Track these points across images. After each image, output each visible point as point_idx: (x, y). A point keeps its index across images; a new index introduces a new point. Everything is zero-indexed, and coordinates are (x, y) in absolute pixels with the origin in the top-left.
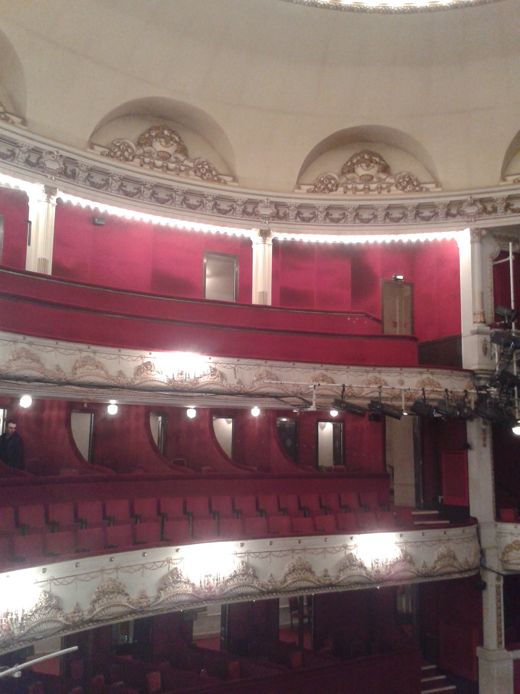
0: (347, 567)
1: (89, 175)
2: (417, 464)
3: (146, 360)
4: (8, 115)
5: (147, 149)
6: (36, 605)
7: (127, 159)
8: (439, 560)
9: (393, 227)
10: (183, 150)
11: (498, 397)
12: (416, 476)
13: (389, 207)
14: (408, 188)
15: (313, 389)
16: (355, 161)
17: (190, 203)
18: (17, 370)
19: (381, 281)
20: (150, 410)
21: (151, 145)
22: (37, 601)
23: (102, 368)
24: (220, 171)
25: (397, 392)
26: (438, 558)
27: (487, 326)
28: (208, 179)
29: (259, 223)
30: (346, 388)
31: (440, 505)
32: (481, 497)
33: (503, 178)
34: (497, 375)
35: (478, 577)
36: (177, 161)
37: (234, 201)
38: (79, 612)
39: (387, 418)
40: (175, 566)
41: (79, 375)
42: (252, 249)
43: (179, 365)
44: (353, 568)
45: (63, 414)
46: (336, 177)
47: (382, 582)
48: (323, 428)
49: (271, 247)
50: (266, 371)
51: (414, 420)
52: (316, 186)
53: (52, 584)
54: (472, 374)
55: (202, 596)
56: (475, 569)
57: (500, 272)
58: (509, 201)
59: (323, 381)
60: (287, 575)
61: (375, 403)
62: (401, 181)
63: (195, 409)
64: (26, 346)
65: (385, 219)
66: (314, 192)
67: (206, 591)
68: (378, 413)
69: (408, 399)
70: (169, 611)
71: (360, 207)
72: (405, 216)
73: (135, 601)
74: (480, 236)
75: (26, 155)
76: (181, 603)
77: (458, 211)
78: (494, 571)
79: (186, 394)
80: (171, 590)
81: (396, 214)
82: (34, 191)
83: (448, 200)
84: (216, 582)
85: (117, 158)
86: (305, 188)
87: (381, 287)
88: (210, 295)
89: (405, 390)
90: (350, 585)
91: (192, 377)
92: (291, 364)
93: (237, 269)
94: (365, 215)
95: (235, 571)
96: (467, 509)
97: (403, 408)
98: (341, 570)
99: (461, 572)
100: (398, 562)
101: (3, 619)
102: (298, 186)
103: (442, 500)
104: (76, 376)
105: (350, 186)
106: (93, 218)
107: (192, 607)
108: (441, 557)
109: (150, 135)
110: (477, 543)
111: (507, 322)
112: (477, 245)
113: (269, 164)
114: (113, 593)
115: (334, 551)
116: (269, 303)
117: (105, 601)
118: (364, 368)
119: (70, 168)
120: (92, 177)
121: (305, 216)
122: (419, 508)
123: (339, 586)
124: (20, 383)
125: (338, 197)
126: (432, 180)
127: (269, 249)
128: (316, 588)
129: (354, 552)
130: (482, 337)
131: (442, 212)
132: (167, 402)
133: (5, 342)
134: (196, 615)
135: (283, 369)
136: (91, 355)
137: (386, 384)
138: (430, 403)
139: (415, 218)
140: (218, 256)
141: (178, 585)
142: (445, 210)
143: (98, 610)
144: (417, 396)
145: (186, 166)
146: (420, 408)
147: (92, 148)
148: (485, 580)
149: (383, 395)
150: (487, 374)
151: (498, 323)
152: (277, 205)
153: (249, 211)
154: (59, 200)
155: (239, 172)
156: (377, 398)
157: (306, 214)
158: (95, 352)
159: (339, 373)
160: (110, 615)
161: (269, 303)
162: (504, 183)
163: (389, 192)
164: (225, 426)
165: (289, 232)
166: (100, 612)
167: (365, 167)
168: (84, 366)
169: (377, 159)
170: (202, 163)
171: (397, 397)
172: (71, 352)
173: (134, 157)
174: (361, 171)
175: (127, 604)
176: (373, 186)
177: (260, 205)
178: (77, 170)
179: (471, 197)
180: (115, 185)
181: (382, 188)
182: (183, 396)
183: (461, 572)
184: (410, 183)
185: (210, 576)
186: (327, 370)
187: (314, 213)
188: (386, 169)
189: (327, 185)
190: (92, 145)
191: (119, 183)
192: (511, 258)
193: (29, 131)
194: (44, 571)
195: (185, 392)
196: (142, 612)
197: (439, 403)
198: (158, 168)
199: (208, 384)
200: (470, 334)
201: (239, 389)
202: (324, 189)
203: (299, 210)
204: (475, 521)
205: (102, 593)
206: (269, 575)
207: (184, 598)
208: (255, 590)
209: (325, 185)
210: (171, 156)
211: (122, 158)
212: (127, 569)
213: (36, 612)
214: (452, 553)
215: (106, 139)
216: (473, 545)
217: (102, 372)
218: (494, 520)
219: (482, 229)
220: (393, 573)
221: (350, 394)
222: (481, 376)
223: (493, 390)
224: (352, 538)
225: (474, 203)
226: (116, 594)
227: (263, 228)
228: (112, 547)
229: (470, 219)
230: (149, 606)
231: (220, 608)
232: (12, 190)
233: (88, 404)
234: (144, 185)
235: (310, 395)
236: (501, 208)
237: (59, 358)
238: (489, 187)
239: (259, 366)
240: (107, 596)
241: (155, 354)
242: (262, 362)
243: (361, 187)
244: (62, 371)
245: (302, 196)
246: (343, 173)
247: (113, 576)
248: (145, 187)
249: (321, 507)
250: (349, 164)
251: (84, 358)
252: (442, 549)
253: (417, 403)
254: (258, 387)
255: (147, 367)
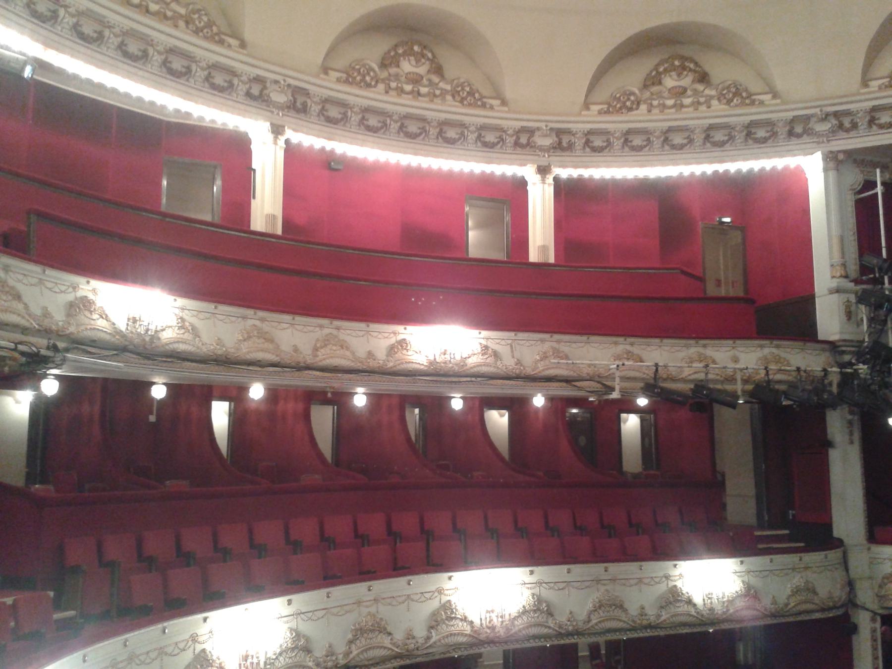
0: (671, 603)
1: (323, 107)
2: (764, 468)
3: (80, 293)
4: (223, 37)
5: (393, 70)
6: (281, 646)
7: (368, 86)
8: (793, 595)
9: (716, 154)
10: (438, 70)
11: (869, 377)
12: (757, 485)
13: (711, 127)
14: (735, 101)
15: (615, 370)
16: (661, 69)
17: (445, 135)
18: (248, 353)
19: (701, 225)
20: (406, 400)
21: (398, 66)
22: (282, 641)
23: (348, 348)
24: (485, 93)
25: (729, 372)
26: (792, 591)
27: (851, 281)
28: (470, 105)
29: (537, 157)
30: (659, 369)
31: (789, 520)
32: (848, 512)
33: (865, 83)
34: (867, 347)
35: (846, 617)
36: (431, 83)
37: (502, 130)
38: (332, 655)
39: (716, 407)
40: (448, 598)
41: (320, 357)
42: (527, 191)
43: (444, 343)
44: (678, 605)
45: (300, 406)
46: (637, 92)
47: (718, 623)
48: (626, 420)
49: (552, 187)
50: (552, 348)
51: (752, 409)
52: (609, 105)
53: (299, 619)
54: (833, 346)
55: (483, 637)
56: (842, 606)
57: (864, 209)
58: (873, 114)
59: (628, 359)
60: (590, 613)
61: (700, 387)
62: (725, 92)
63: (461, 398)
64: (258, 323)
65: (704, 144)
66: (607, 112)
67: (488, 631)
68: (703, 401)
69: (745, 381)
70: (442, 656)
71: (670, 130)
72: (731, 138)
73: (400, 643)
74: (834, 161)
75: (247, 86)
76: (458, 646)
77: (804, 128)
78: (867, 610)
79: (450, 379)
80: (444, 629)
81: (719, 136)
82: (255, 128)
83: (791, 114)
84: (500, 620)
85: (357, 84)
86: (595, 108)
87: (700, 231)
88: (474, 251)
89: (741, 370)
90: (675, 627)
91: (458, 358)
92: (584, 338)
93: (508, 218)
94: (678, 139)
95: (524, 607)
96: (829, 526)
97: (739, 393)
98: (662, 607)
99: (823, 610)
100: (739, 596)
101: (242, 663)
102: (586, 106)
103: (793, 516)
104: (318, 359)
105: (655, 103)
106: (329, 163)
107: (471, 652)
108: (796, 591)
109: (396, 53)
110: (844, 573)
111: (877, 275)
112: (832, 174)
113: (546, 78)
114: (372, 631)
115: (652, 583)
116: (552, 260)
117: (362, 642)
118: (683, 342)
119: (300, 100)
120: (327, 111)
121: (596, 145)
122: (761, 527)
123: (661, 628)
124: (251, 368)
125: (640, 118)
126: (767, 89)
127: (550, 190)
128: (629, 630)
129: (679, 584)
130: (844, 297)
131: (782, 131)
132: (429, 390)
133: (233, 319)
134: (476, 662)
135: (574, 345)
136: (335, 332)
137: (714, 362)
138: (777, 387)
139: (746, 140)
140: (482, 203)
141: (452, 623)
142: (787, 128)
143: (355, 653)
144: (758, 377)
145: (442, 89)
146: (763, 394)
147: (326, 73)
148: (855, 621)
149: (710, 376)
150: (853, 346)
151: (864, 278)
152: (559, 132)
153: (522, 142)
154: (287, 142)
155: (509, 93)
156: (702, 381)
157: (598, 142)
158: (338, 328)
159: (649, 349)
160: (368, 660)
161: (552, 260)
162: (866, 90)
163: (709, 107)
164: (498, 421)
165: (576, 167)
166: (358, 655)
167: (675, 77)
168: (326, 345)
169: (692, 66)
170: (462, 85)
171: (731, 380)
172: (312, 328)
173: (377, 82)
174: (670, 82)
175: (390, 646)
176: (687, 101)
177: (537, 133)
178: (309, 101)
179: (821, 111)
180: (355, 119)
181: (699, 103)
182: (448, 382)
183: (823, 610)
184: (736, 94)
185: (493, 611)
186: (632, 344)
187: (608, 141)
188: (703, 78)
189: (625, 103)
190: (325, 70)
191: (360, 116)
192: (879, 189)
193: (249, 55)
194: (290, 602)
195: (450, 376)
196: (408, 656)
197: (790, 386)
198: (408, 93)
199: (478, 366)
200: (826, 292)
201: (518, 372)
202: (621, 108)
203: (588, 137)
204: (838, 543)
205: (360, 632)
206: (568, 612)
207: (461, 639)
208: (551, 631)
209: (622, 104)
210: (422, 77)
211: (362, 84)
212: (389, 601)
213: (280, 654)
214: (810, 585)
215: (342, 62)
216: (839, 575)
217: (348, 353)
218: (865, 542)
219: (839, 152)
220: (731, 611)
221: (665, 376)
222: (844, 349)
223: (863, 368)
224: (675, 566)
225: (826, 117)
226: (377, 633)
227: (541, 164)
228: (369, 572)
229: (821, 140)
230: (417, 649)
231: (501, 656)
232: (230, 131)
233: (333, 393)
234: (390, 117)
235: (612, 377)
236: (863, 124)
237: (297, 336)
238: (845, 96)
239: (543, 341)
240: (365, 635)
241: (411, 329)
242: (546, 336)
243: (670, 102)
244: (301, 353)
245: (594, 119)
246: (645, 86)
247: (373, 610)
248: (391, 120)
249: (630, 524)
250: (654, 73)
251: (327, 335)
252: (797, 580)
253: (758, 386)
254: (542, 369)
255: (402, 346)
